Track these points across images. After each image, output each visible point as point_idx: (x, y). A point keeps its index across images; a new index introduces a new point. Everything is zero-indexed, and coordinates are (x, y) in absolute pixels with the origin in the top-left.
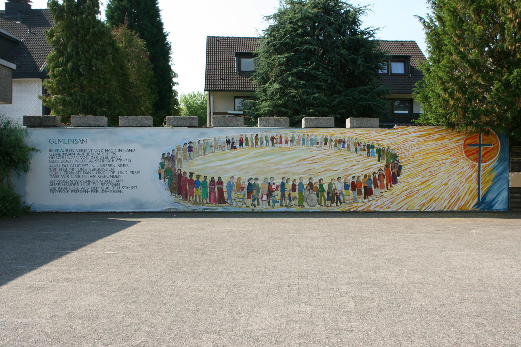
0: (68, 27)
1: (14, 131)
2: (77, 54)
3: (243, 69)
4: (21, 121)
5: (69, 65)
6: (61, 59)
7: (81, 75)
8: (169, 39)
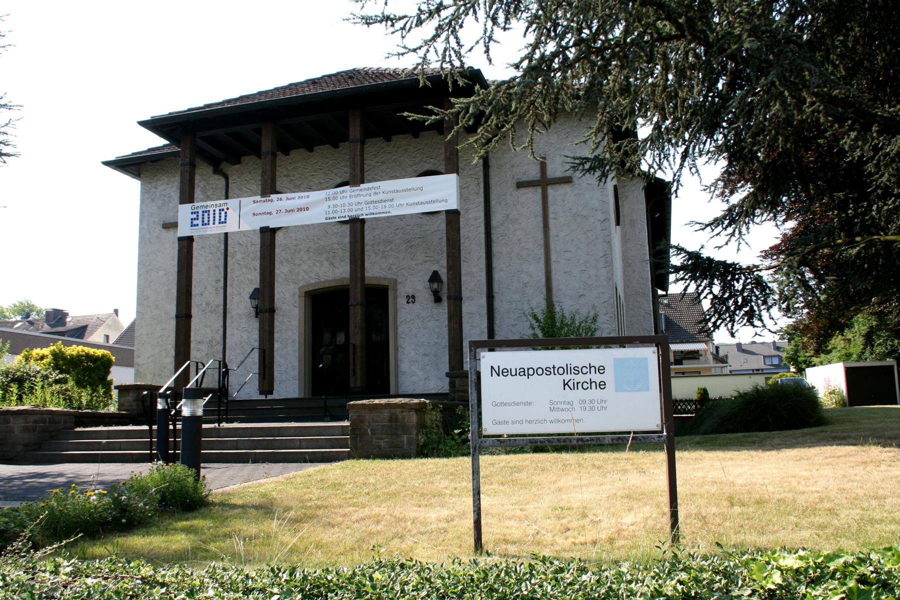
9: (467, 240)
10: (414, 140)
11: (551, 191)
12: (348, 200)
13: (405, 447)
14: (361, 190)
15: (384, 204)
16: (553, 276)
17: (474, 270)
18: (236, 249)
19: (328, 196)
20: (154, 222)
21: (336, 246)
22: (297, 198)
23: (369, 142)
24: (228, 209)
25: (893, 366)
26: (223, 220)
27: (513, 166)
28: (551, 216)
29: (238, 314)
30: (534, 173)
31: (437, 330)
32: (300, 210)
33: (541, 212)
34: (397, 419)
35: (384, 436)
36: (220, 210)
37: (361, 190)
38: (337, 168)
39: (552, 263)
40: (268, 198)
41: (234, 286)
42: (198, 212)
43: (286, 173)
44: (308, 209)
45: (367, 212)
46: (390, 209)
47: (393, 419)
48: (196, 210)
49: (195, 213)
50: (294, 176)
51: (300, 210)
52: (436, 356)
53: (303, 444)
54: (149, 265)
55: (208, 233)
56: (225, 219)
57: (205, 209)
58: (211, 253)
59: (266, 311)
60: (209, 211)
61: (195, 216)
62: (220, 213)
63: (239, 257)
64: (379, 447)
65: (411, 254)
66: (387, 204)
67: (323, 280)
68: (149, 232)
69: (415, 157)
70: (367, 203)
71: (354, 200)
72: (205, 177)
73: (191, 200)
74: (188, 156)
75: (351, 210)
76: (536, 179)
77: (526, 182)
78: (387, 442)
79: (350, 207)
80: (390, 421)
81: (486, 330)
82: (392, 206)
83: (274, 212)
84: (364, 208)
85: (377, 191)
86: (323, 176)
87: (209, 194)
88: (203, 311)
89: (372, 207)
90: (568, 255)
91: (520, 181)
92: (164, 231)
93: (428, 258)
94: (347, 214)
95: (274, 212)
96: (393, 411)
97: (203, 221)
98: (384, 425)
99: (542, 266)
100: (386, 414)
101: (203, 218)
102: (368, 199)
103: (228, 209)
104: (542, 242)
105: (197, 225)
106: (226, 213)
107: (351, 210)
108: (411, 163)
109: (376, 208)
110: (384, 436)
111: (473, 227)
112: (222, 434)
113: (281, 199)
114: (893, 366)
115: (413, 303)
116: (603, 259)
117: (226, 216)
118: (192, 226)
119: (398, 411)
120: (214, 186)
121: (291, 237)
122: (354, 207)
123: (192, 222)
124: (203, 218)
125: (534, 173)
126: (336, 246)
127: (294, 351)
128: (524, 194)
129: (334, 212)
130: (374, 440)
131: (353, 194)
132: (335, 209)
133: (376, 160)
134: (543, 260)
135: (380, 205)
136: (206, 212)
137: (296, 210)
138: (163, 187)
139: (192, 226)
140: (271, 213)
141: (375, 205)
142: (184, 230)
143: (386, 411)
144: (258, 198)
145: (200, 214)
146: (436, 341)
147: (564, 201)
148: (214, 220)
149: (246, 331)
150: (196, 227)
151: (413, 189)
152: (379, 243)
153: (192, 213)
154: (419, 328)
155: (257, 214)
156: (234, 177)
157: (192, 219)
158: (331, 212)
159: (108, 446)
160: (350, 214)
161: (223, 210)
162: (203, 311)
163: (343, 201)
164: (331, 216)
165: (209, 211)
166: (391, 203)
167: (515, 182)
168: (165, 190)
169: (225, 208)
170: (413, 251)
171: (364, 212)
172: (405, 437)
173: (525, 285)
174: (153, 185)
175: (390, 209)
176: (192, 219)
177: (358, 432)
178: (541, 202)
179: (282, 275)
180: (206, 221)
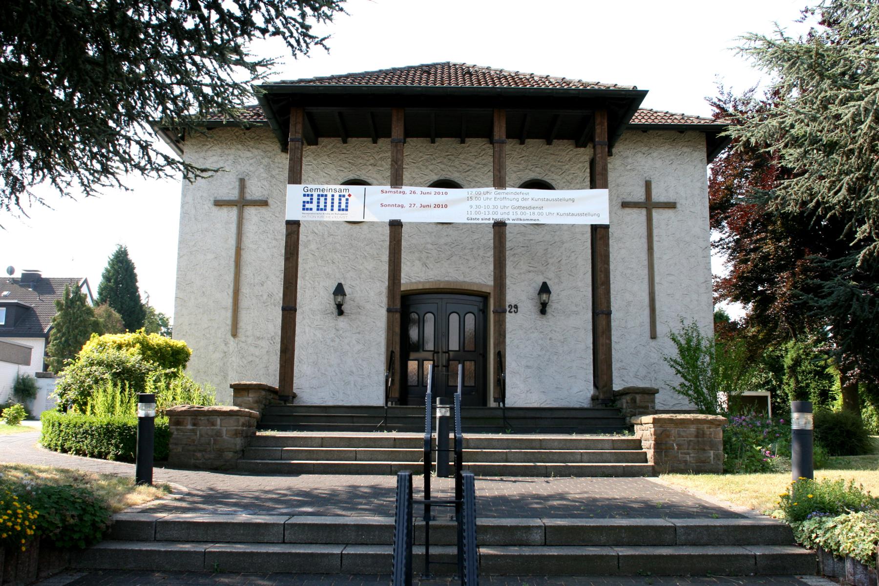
0: (65, 315)
1: (31, 380)
2: (69, 332)
3: (466, 349)
4: (34, 375)
5: (63, 339)
6: (58, 335)
7: (70, 345)
8: (136, 271)
9: (573, 254)
10: (518, 146)
11: (656, 214)
12: (492, 203)
13: (712, 462)
14: (507, 194)
15: (532, 211)
16: (657, 298)
17: (580, 284)
18: (310, 238)
19: (470, 196)
20: (202, 196)
21: (429, 246)
22: (433, 193)
23: (412, 142)
24: (350, 195)
25: (767, 397)
26: (343, 206)
27: (618, 185)
28: (655, 239)
29: (311, 310)
30: (639, 195)
31: (540, 342)
32: (437, 206)
33: (646, 234)
34: (704, 433)
35: (691, 451)
36: (340, 196)
37: (507, 194)
38: (432, 164)
39: (656, 285)
40: (399, 190)
41: (307, 278)
42: (312, 195)
43: (372, 161)
44: (446, 206)
45: (514, 217)
46: (540, 217)
47: (700, 434)
48: (309, 193)
49: (308, 195)
50: (382, 166)
51: (437, 206)
52: (539, 368)
53: (585, 457)
54: (194, 246)
55: (325, 220)
56: (347, 206)
57: (321, 193)
58: (275, 239)
59: (396, 312)
60: (326, 195)
61: (308, 199)
62: (340, 200)
63: (313, 246)
64: (686, 462)
65: (514, 262)
66: (536, 211)
67: (414, 281)
68: (195, 208)
69: (518, 164)
70: (514, 208)
71: (499, 203)
72: (269, 154)
73: (298, 181)
74: (300, 131)
75: (495, 213)
76: (640, 201)
77: (631, 202)
78: (693, 457)
79: (495, 210)
80: (697, 436)
81: (591, 346)
82: (541, 214)
83: (407, 206)
84: (511, 213)
85: (525, 196)
86: (416, 170)
87: (274, 173)
88: (264, 303)
89: (519, 213)
90: (671, 278)
91: (625, 201)
92: (215, 209)
93: (532, 269)
94: (491, 216)
95: (407, 206)
96: (701, 426)
97: (318, 206)
98: (690, 441)
99: (645, 286)
100: (692, 429)
101: (318, 203)
102: (517, 204)
103: (350, 195)
104: (646, 263)
105: (311, 209)
106: (347, 200)
107: (495, 213)
108: (515, 169)
109: (523, 213)
110: (691, 451)
111: (579, 241)
112: (472, 445)
113: (414, 193)
114: (767, 397)
115: (516, 312)
116: (704, 285)
117: (347, 203)
118: (304, 209)
119: (705, 426)
120: (280, 166)
121: (377, 232)
122: (500, 211)
123: (304, 206)
124: (318, 203)
125: (639, 195)
126: (429, 246)
127: (379, 354)
128: (629, 214)
129: (477, 213)
130: (680, 455)
131: (498, 196)
132: (478, 210)
133: (476, 161)
134: (646, 281)
135: (528, 211)
136: (322, 196)
137: (433, 206)
138: (215, 158)
139: (304, 209)
140: (402, 206)
141: (523, 211)
142: (293, 212)
143: (692, 426)
144: (388, 188)
145: (315, 198)
146: (540, 353)
147: (667, 225)
148: (332, 206)
149: (320, 329)
150: (309, 212)
151: (564, 200)
152: (479, 248)
153: (304, 195)
154: (522, 339)
155: (386, 206)
156: (308, 159)
157: (304, 202)
158: (491, 213)
159: (593, 458)
160: (495, 217)
161: (344, 196)
162: (264, 303)
163: (488, 202)
164: (474, 216)
165: (326, 195)
166: (541, 211)
167: (620, 201)
168: (217, 162)
169: (347, 194)
170: (516, 259)
171: (510, 218)
172: (712, 452)
173: (629, 303)
174: (203, 154)
175: (540, 217)
176: (304, 202)
177: (663, 447)
178: (645, 224)
179: (365, 271)
180: (322, 206)
